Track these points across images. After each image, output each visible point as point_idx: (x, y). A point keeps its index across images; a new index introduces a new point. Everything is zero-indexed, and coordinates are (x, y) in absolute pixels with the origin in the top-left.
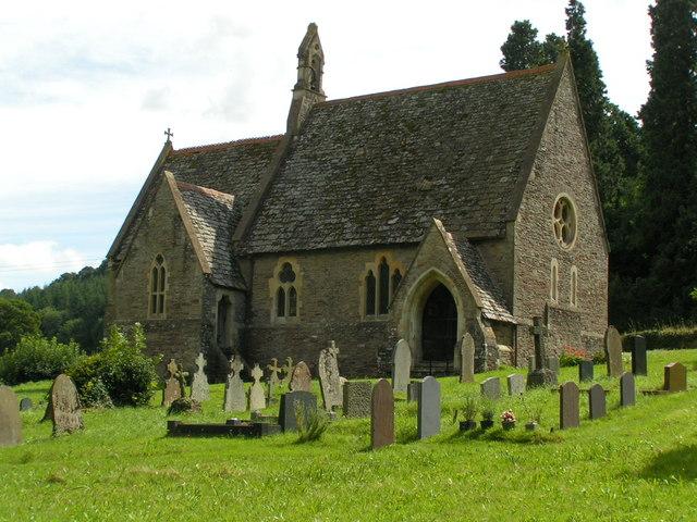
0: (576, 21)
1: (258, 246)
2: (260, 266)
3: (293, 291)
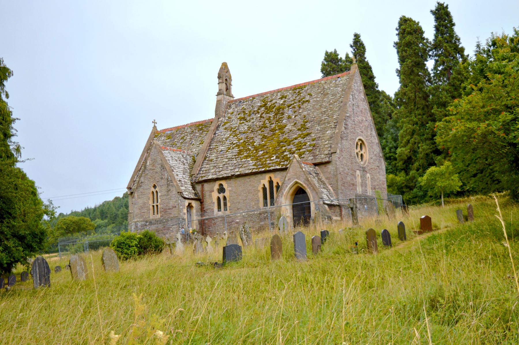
2: (207, 186)
3: (225, 198)
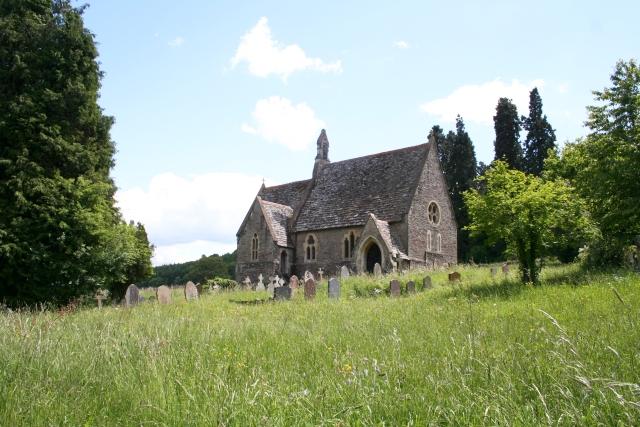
0: (460, 125)
1: (300, 228)
2: (299, 237)
3: (314, 248)
